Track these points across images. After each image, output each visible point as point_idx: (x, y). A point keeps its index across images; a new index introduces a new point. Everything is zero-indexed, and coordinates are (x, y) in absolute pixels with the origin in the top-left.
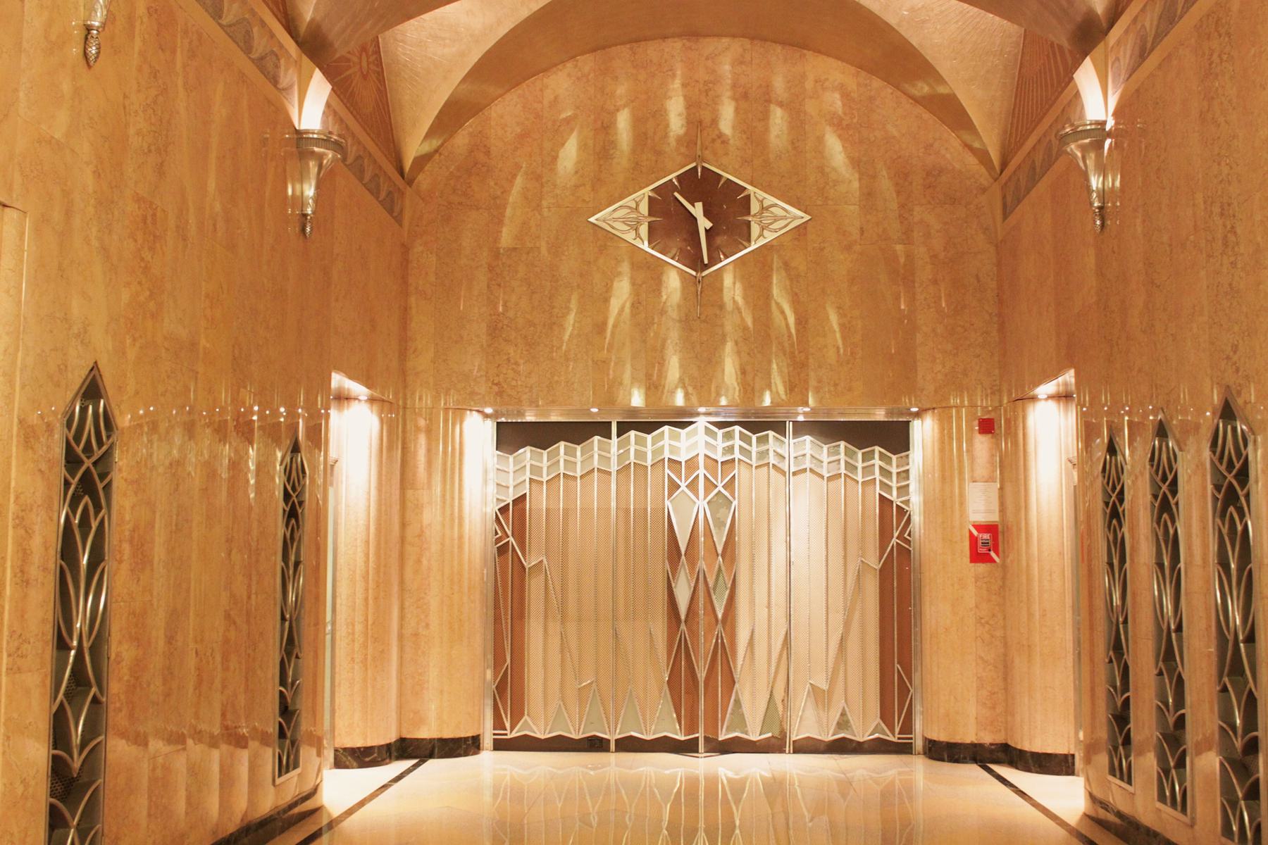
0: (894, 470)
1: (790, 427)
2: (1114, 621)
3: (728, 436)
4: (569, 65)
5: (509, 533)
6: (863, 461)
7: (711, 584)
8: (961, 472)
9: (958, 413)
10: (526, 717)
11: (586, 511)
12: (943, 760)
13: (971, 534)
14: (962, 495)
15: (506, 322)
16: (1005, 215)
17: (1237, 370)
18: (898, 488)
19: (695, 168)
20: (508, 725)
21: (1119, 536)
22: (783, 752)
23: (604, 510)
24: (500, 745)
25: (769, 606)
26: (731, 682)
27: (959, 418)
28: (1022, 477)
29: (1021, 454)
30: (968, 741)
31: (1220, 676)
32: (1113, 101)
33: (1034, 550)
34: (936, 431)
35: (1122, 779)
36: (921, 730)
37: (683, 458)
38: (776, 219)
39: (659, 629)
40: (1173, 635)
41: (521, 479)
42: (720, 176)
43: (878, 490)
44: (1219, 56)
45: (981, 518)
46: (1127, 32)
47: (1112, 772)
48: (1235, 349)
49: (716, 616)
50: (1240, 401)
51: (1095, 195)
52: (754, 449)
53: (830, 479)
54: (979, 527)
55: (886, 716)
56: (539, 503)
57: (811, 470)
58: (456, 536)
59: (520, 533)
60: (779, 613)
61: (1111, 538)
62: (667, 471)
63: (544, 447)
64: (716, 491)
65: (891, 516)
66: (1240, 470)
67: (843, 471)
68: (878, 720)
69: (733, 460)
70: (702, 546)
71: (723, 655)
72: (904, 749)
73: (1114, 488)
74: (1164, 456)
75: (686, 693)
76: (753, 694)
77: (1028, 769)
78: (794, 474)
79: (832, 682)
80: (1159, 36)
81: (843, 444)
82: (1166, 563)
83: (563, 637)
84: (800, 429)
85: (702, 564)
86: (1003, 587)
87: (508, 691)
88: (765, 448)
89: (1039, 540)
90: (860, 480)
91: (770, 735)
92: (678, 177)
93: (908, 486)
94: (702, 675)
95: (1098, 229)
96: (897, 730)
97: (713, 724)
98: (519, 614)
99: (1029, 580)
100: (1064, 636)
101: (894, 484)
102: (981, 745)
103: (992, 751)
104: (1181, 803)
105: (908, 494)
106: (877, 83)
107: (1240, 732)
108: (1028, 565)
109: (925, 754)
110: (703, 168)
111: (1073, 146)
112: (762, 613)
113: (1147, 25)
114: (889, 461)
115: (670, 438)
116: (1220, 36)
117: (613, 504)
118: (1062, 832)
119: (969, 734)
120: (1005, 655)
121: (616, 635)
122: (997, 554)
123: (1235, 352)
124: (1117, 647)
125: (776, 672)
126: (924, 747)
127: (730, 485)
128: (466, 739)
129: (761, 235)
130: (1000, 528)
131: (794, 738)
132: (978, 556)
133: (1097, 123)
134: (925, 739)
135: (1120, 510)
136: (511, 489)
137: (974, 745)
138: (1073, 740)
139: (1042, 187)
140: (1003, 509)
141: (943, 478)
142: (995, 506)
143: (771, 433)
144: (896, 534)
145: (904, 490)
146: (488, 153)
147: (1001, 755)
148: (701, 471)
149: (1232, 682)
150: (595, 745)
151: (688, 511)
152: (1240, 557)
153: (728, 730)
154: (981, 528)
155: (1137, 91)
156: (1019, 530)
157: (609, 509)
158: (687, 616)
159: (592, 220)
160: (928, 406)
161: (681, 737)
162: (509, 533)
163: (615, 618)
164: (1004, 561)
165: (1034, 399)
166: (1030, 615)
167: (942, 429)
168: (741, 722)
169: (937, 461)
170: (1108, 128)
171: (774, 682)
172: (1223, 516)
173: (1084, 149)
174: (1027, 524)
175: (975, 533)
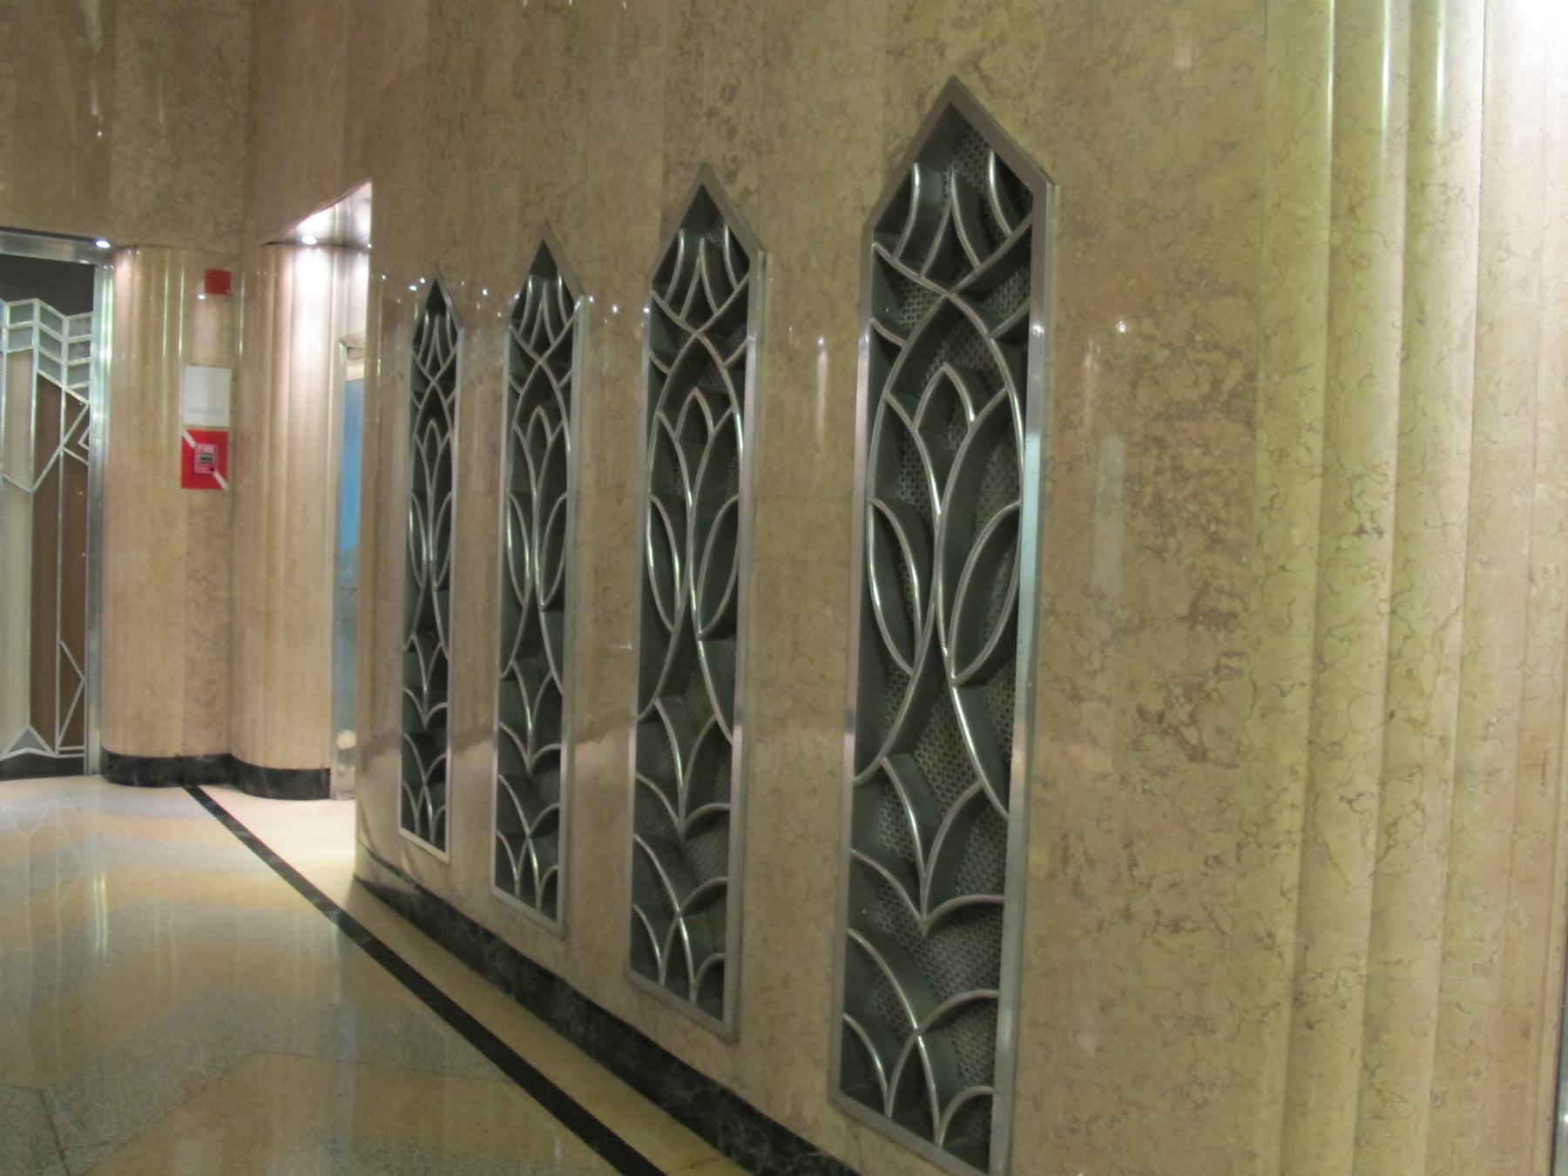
0: (65, 338)
2: (422, 585)
6: (12, 321)
13: (185, 444)
17: (732, 133)
18: (71, 369)
21: (441, 446)
30: (170, 754)
33: (282, 472)
34: (138, 277)
36: (95, 745)
40: (435, 595)
43: (36, 369)
45: (202, 421)
47: (408, 822)
48: (730, 94)
50: (732, 192)
54: (199, 435)
55: (40, 719)
61: (424, 450)
65: (55, 411)
66: (720, 321)
72: (69, 767)
73: (435, 367)
74: (544, 305)
77: (261, 793)
82: (535, 494)
89: (291, 456)
96: (58, 740)
100: (324, 602)
101: (64, 361)
103: (207, 767)
104: (546, 895)
105: (86, 377)
107: (683, 797)
109: (103, 772)
114: (57, 325)
118: (333, 928)
119: (172, 743)
122: (224, 475)
123: (729, 100)
124: (426, 627)
126: (102, 762)
130: (230, 438)
132: (193, 478)
135: (445, 403)
137: (179, 760)
141: (144, 356)
142: (225, 404)
144: (64, 440)
147: (221, 772)
149: (666, 706)
154: (201, 436)
156: (261, 440)
160: (126, 242)
165: (295, 244)
166: (272, 569)
167: (147, 281)
169: (135, 329)
172: (672, 407)
174: (272, 433)
175: (192, 443)
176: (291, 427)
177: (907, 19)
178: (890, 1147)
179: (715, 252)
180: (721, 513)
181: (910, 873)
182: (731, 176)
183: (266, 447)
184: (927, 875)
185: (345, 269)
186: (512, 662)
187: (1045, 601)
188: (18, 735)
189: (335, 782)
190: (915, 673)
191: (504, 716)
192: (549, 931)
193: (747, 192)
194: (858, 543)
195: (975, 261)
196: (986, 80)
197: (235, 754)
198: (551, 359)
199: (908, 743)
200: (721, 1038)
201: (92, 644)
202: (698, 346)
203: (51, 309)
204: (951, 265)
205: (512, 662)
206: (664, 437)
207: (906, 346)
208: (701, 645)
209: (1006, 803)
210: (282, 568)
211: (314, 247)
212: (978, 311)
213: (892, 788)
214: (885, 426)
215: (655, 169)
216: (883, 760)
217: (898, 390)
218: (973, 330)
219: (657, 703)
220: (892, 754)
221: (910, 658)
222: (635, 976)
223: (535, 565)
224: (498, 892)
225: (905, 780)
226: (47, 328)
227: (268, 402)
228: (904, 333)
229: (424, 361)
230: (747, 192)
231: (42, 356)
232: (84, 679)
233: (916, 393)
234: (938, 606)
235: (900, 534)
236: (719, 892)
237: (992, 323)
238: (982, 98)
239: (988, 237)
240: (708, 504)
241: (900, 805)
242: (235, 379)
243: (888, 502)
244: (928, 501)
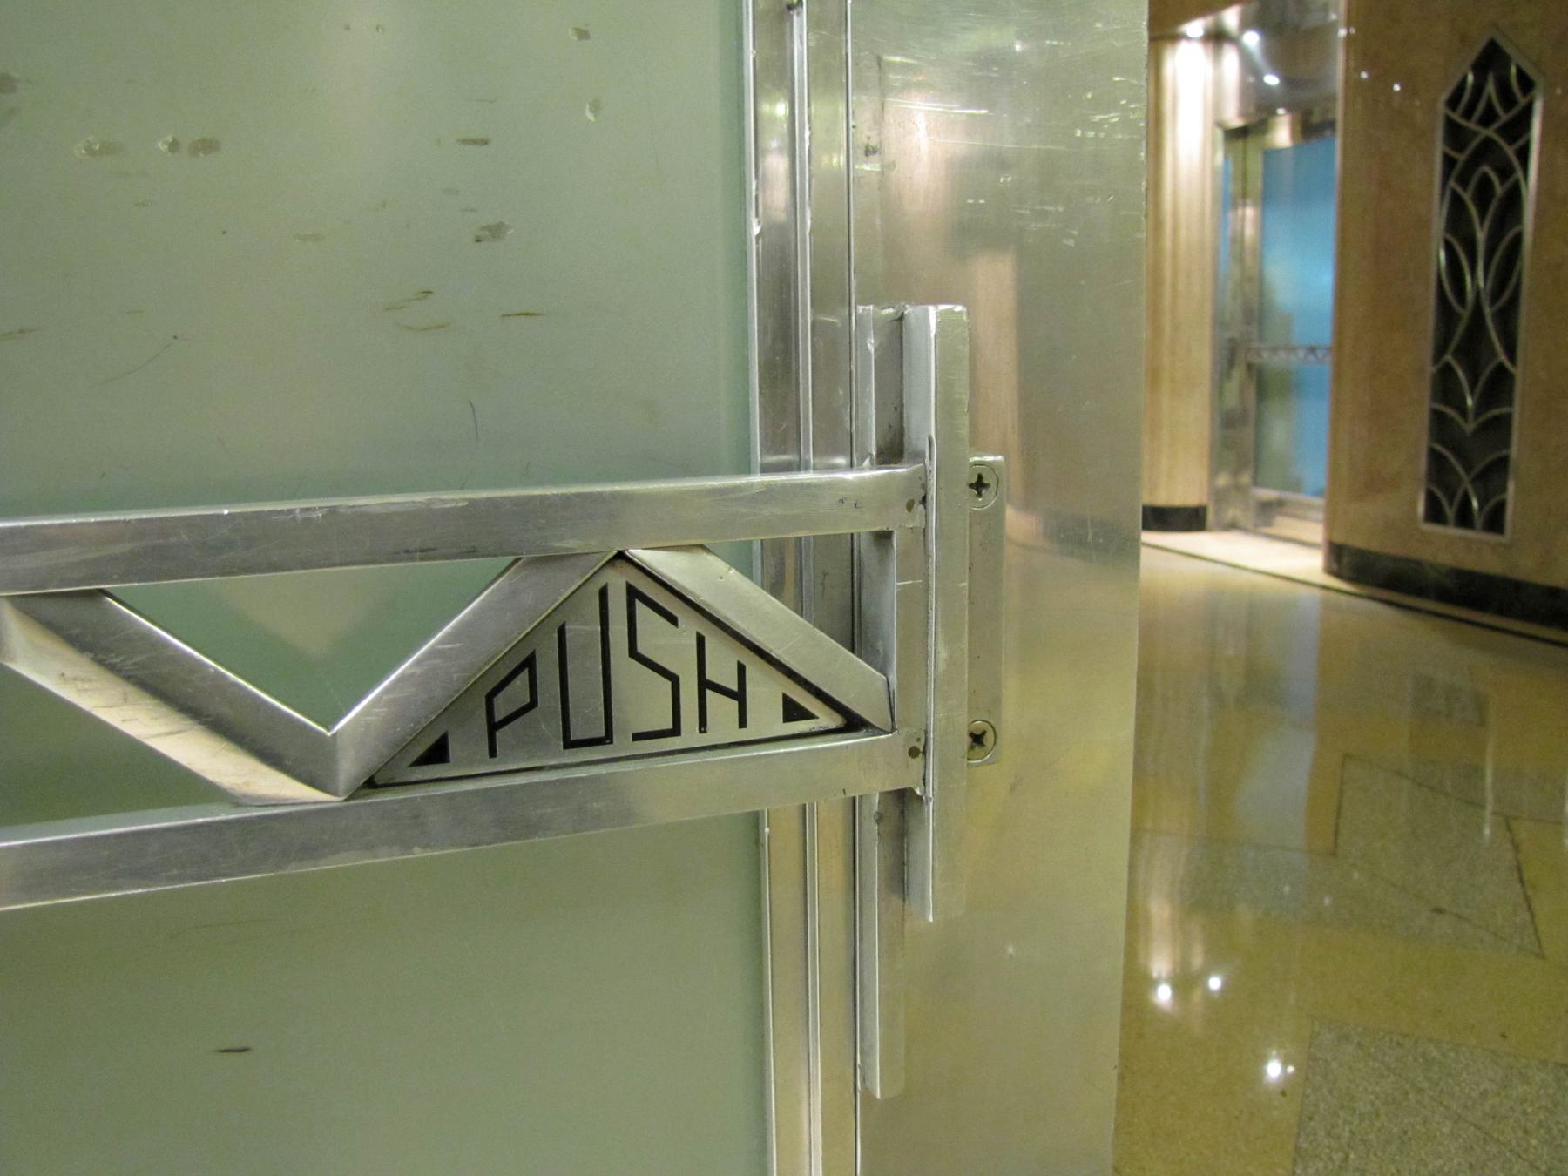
33: (1167, 244)
185: (1217, 56)
189: (1211, 517)
210: (1167, 329)
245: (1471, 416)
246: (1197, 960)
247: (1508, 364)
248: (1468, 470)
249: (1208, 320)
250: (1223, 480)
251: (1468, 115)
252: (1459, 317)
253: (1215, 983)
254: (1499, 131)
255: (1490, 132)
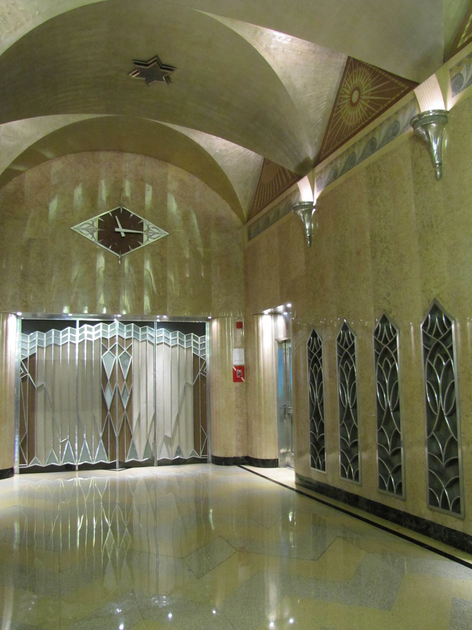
1: (156, 325)
2: (315, 405)
3: (129, 328)
4: (63, 158)
5: (27, 371)
6: (186, 339)
7: (121, 394)
8: (229, 344)
9: (228, 320)
10: (35, 457)
11: (65, 361)
12: (222, 465)
13: (233, 370)
14: (229, 353)
15: (30, 273)
16: (250, 238)
17: (390, 303)
18: (201, 351)
19: (119, 209)
20: (27, 462)
22: (153, 466)
23: (73, 360)
24: (22, 471)
25: (147, 402)
26: (130, 436)
27: (228, 322)
28: (256, 347)
29: (256, 337)
30: (233, 456)
31: (379, 426)
32: (317, 195)
33: (262, 376)
34: (219, 327)
35: (319, 468)
37: (108, 337)
38: (154, 233)
39: (98, 413)
41: (34, 346)
42: (130, 213)
43: (193, 352)
44: (380, 179)
46: (326, 167)
48: (388, 295)
49: (123, 407)
50: (391, 316)
51: (308, 231)
52: (140, 333)
53: (172, 347)
55: (196, 447)
56: (42, 356)
57: (165, 343)
58: (4, 373)
59: (33, 372)
60: (151, 406)
61: (313, 371)
62: (101, 343)
63: (45, 332)
64: (124, 352)
65: (198, 362)
67: (178, 343)
68: (193, 449)
69: (131, 338)
70: (117, 376)
71: (126, 425)
72: (203, 461)
74: (346, 337)
75: (110, 442)
76: (140, 441)
78: (158, 344)
79: (173, 435)
80: (344, 170)
81: (178, 332)
83: (53, 420)
84: (161, 325)
85: (117, 385)
86: (246, 392)
87: (28, 446)
88: (145, 333)
90: (185, 347)
91: (147, 459)
92: (112, 212)
93: (205, 350)
94: (117, 434)
95: (309, 246)
97: (123, 456)
98: (32, 409)
99: (260, 388)
101: (199, 349)
102: (238, 458)
103: (242, 460)
106: (197, 180)
107: (390, 447)
108: (259, 383)
110: (123, 209)
111: (299, 212)
112: (143, 406)
113: (339, 166)
114: (197, 339)
115: (103, 328)
116: (380, 172)
117: (77, 357)
118: (295, 493)
119: (233, 453)
120: (247, 420)
121: (78, 417)
122: (244, 378)
123: (388, 296)
125: (150, 431)
127: (130, 349)
128: (8, 470)
129: (148, 240)
131: (158, 459)
132: (236, 379)
133: (309, 202)
134: (213, 457)
136: (28, 351)
137: (235, 458)
138: (277, 453)
139: (273, 228)
140: (246, 359)
142: (243, 358)
143: (147, 327)
144: (200, 370)
145: (203, 351)
146: (23, 194)
147: (246, 461)
148: (117, 343)
150: (69, 468)
151: (110, 361)
152: (318, 379)
153: (129, 458)
154: (238, 367)
155: (331, 191)
156: (255, 369)
157: (75, 360)
158: (111, 408)
159: (72, 228)
161: (108, 462)
162: (27, 371)
163: (77, 410)
164: (246, 381)
166: (260, 403)
168: (135, 453)
169: (219, 340)
170: (314, 204)
171: (149, 436)
173: (303, 213)
175: (235, 369)
176: (263, 364)
177: (425, 285)
178: (441, 515)
179: (388, 328)
180: (394, 384)
181: (440, 456)
182: (390, 312)
183: (257, 370)
184: (443, 455)
185: (275, 319)
186: (343, 421)
187: (461, 399)
188: (190, 452)
189: (280, 463)
190: (438, 415)
191: (342, 435)
192: (357, 485)
193: (394, 316)
194: (424, 389)
195: (442, 334)
196: (441, 299)
197: (250, 456)
198: (349, 350)
199: (438, 429)
200: (402, 500)
201: (208, 427)
202: (386, 348)
203: (196, 336)
204: (437, 335)
205: (343, 421)
206: (379, 368)
207: (430, 350)
208: (392, 413)
209: (457, 438)
210: (263, 403)
211: (267, 315)
212: (444, 343)
213: (435, 439)
214: (428, 366)
215: (372, 309)
216: (433, 433)
217: (429, 359)
218: (442, 347)
219: (382, 427)
220: (435, 431)
221: (436, 412)
222: (381, 490)
223: (348, 399)
224: (342, 478)
225: (438, 438)
226: (194, 341)
227: (257, 357)
228: (430, 347)
229: (312, 349)
230: (394, 316)
231: (194, 348)
232: (207, 436)
233: (433, 359)
234: (441, 402)
235: (432, 387)
236: (400, 467)
237: (446, 346)
238: (440, 302)
239: (444, 329)
240: (391, 382)
241: (437, 442)
242: (245, 351)
243: (430, 381)
244: (437, 380)
245: (349, 441)
246: (286, 614)
247: (454, 437)
248: (350, 459)
249: (276, 400)
250: (282, 451)
251: (380, 340)
252: (436, 416)
253: (291, 621)
254: (388, 346)
255: (438, 340)
